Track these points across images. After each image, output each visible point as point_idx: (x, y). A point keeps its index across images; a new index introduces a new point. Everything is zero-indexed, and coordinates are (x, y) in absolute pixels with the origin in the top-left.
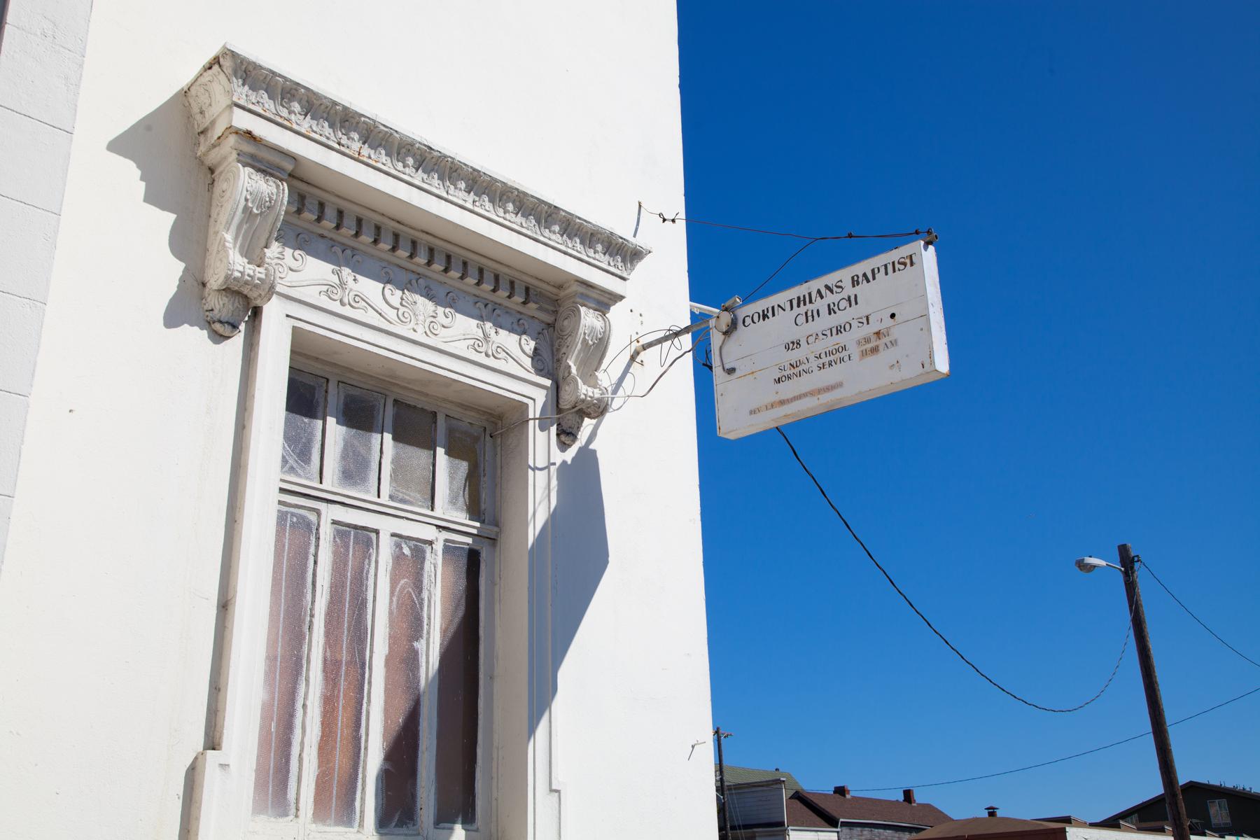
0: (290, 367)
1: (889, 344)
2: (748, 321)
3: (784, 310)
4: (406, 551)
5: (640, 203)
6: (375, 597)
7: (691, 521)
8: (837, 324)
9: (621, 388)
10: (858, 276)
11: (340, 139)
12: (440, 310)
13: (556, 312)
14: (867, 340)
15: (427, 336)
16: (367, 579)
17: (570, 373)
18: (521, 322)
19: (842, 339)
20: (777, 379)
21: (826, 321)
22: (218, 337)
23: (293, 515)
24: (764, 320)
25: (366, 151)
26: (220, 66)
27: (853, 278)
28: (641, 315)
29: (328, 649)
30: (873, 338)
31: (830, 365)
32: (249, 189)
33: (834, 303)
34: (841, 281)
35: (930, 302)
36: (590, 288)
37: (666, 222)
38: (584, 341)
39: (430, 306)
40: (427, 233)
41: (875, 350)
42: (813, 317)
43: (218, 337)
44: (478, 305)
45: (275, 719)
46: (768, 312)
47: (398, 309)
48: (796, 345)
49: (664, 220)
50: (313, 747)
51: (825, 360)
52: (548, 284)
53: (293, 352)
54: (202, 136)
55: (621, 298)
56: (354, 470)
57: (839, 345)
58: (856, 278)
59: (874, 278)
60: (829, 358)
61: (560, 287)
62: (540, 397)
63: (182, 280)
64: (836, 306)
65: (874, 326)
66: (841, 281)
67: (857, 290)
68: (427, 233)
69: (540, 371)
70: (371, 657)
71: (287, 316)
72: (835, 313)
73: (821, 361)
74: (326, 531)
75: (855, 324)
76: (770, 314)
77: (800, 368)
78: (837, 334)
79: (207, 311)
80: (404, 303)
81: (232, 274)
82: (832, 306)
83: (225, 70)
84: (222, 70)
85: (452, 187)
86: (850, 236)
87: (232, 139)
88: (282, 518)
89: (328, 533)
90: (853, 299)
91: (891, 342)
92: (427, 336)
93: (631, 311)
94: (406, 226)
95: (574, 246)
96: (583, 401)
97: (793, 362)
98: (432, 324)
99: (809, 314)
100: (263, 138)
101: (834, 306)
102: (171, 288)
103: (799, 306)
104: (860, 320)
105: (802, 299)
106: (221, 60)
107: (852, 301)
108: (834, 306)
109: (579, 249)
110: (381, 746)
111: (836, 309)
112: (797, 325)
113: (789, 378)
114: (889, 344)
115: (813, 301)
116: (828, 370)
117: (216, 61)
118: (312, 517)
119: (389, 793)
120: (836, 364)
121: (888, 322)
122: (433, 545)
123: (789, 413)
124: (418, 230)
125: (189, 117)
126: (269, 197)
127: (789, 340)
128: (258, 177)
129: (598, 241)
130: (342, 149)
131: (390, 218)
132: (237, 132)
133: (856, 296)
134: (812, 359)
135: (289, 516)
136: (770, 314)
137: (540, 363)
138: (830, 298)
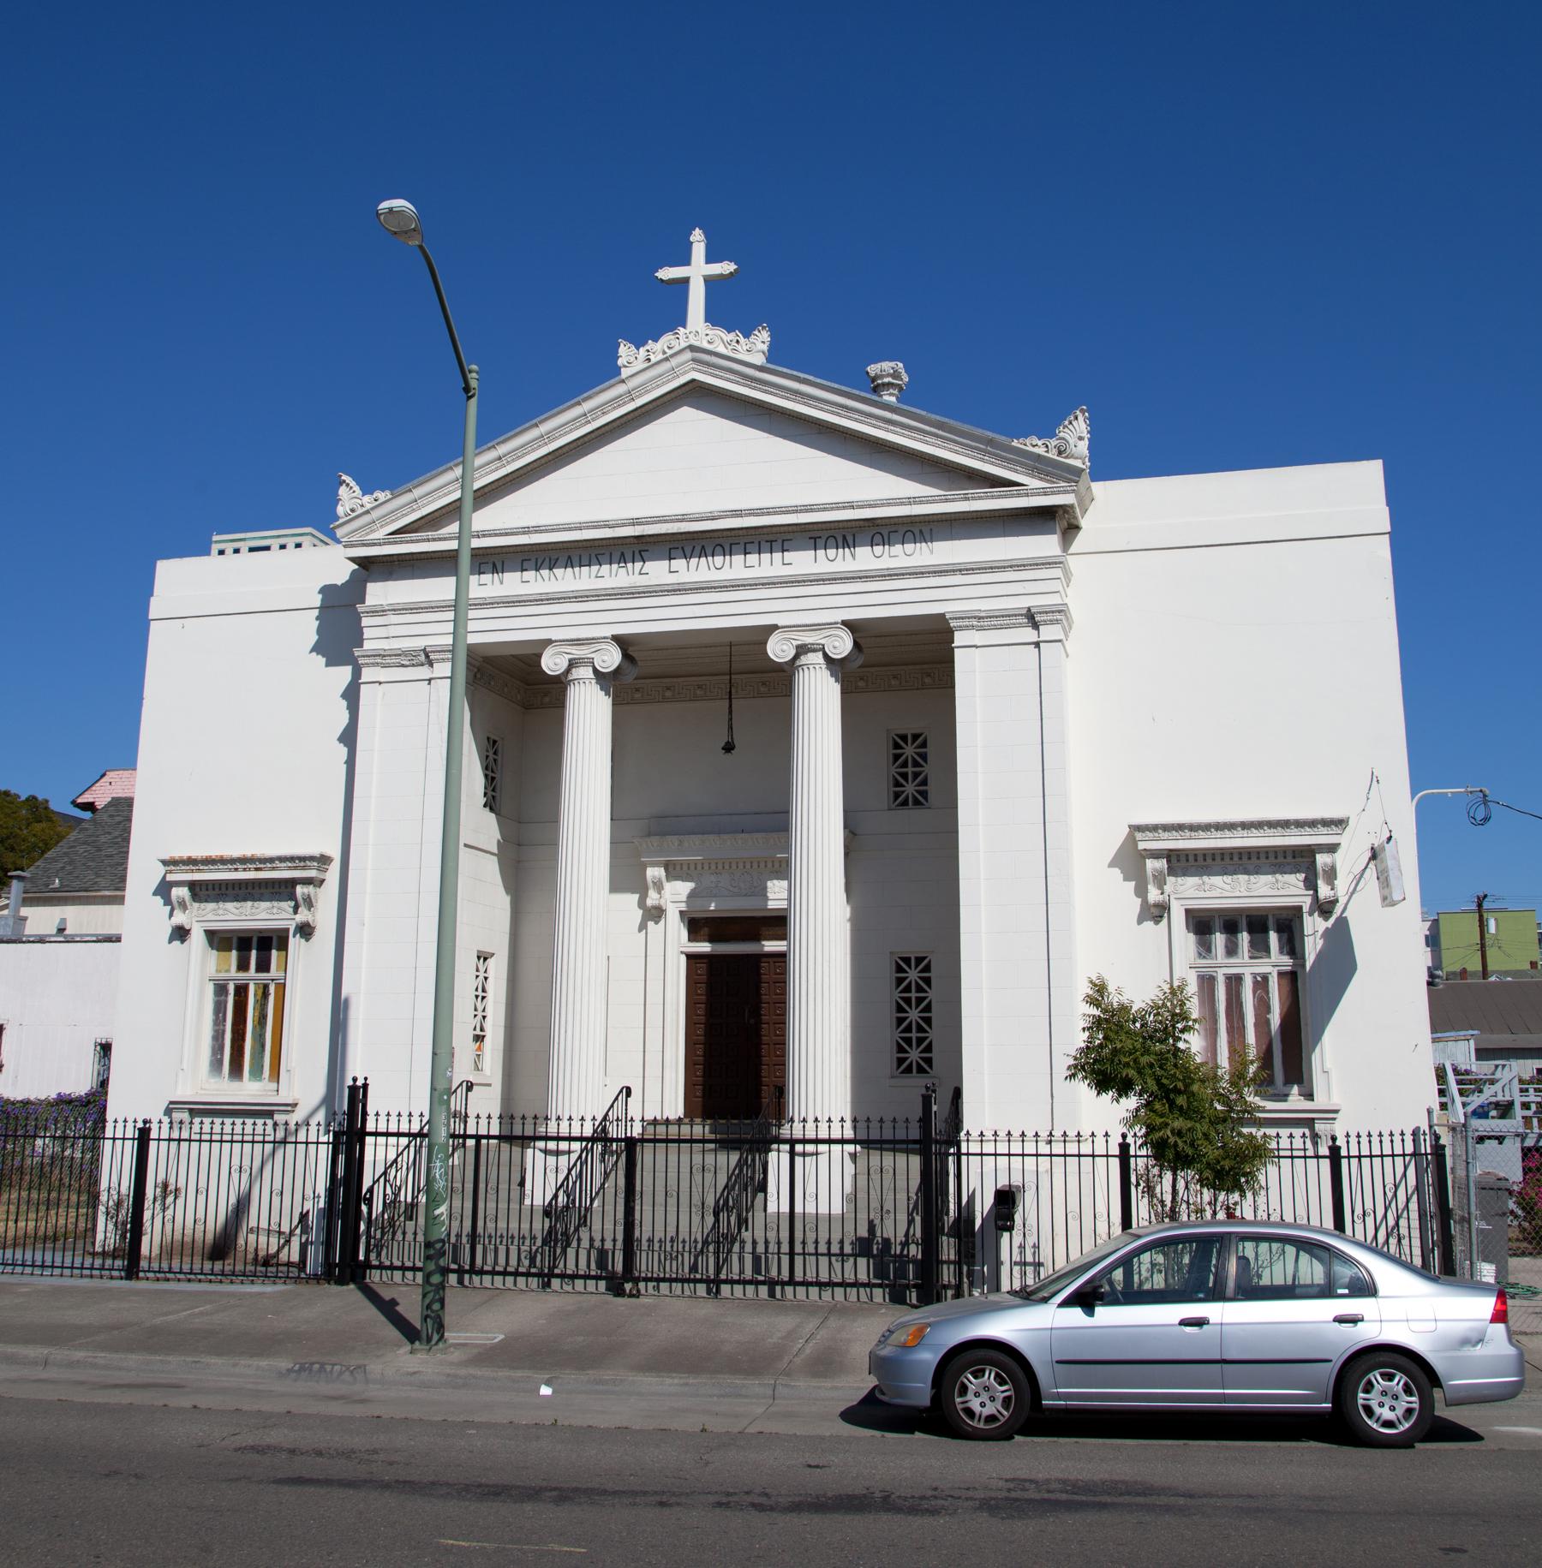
4: (1259, 979)
11: (296, 909)
12: (1252, 877)
22: (1157, 923)
25: (1193, 834)
38: (1323, 870)
39: (1246, 877)
43: (1157, 923)
56: (1231, 950)
62: (1308, 900)
63: (1141, 905)
69: (1307, 888)
91: (1187, 860)
102: (1137, 909)
118: (1215, 974)
128: (1156, 861)
129: (1264, 825)
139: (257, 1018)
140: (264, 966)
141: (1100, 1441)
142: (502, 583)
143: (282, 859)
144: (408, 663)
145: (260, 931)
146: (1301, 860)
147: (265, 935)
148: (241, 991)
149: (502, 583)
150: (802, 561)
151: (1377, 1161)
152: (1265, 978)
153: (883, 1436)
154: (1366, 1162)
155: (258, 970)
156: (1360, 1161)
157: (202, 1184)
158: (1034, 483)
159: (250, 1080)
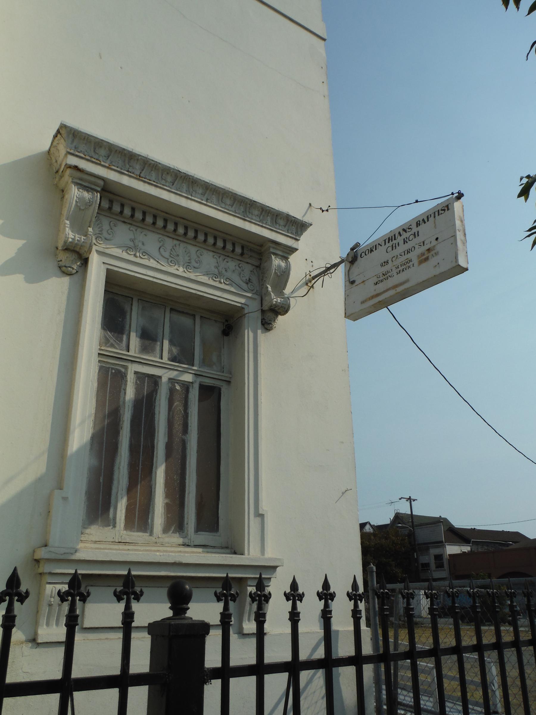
0: (105, 291)
1: (434, 255)
2: (363, 254)
3: (381, 246)
4: (178, 387)
7: (343, 370)
8: (406, 249)
10: (419, 221)
13: (261, 259)
14: (423, 254)
15: (186, 272)
16: (155, 403)
17: (268, 290)
18: (240, 265)
19: (409, 256)
20: (375, 283)
21: (402, 248)
23: (112, 369)
24: (371, 253)
26: (60, 134)
27: (417, 223)
28: (312, 262)
30: (426, 253)
31: (403, 271)
32: (77, 196)
33: (407, 238)
34: (411, 225)
35: (457, 228)
36: (277, 245)
37: (324, 212)
38: (275, 273)
40: (183, 219)
41: (427, 259)
42: (396, 246)
44: (215, 256)
45: (102, 475)
46: (373, 248)
47: (168, 259)
48: (386, 263)
49: (323, 211)
50: (124, 490)
51: (401, 268)
52: (254, 244)
53: (107, 282)
54: (57, 174)
55: (296, 250)
57: (408, 260)
58: (418, 222)
59: (428, 220)
60: (403, 267)
61: (261, 246)
64: (408, 239)
65: (427, 247)
66: (411, 225)
68: (183, 219)
70: (157, 444)
71: (104, 263)
72: (407, 242)
73: (398, 270)
74: (131, 378)
75: (417, 247)
76: (374, 249)
77: (388, 275)
78: (408, 253)
79: (58, 261)
80: (171, 256)
81: (68, 240)
82: (406, 239)
83: (63, 136)
84: (62, 137)
85: (194, 192)
86: (417, 201)
87: (68, 171)
88: (101, 368)
89: (132, 378)
90: (416, 234)
92: (186, 272)
93: (306, 260)
94: (171, 215)
95: (266, 222)
96: (275, 305)
97: (384, 273)
98: (188, 267)
99: (394, 245)
100: (84, 169)
101: (407, 239)
103: (389, 242)
104: (420, 244)
105: (391, 238)
106: (60, 130)
108: (407, 239)
109: (270, 224)
110: (164, 490)
111: (408, 240)
112: (387, 252)
113: (382, 281)
114: (434, 255)
115: (396, 238)
116: (402, 274)
117: (58, 132)
119: (169, 515)
120: (406, 270)
121: (434, 243)
122: (193, 385)
123: (380, 300)
124: (178, 217)
125: (51, 165)
126: (89, 200)
127: (383, 262)
130: (130, 174)
131: (161, 211)
132: (70, 167)
133: (418, 232)
134: (394, 268)
135: (110, 369)
136: (374, 249)
137: (252, 287)
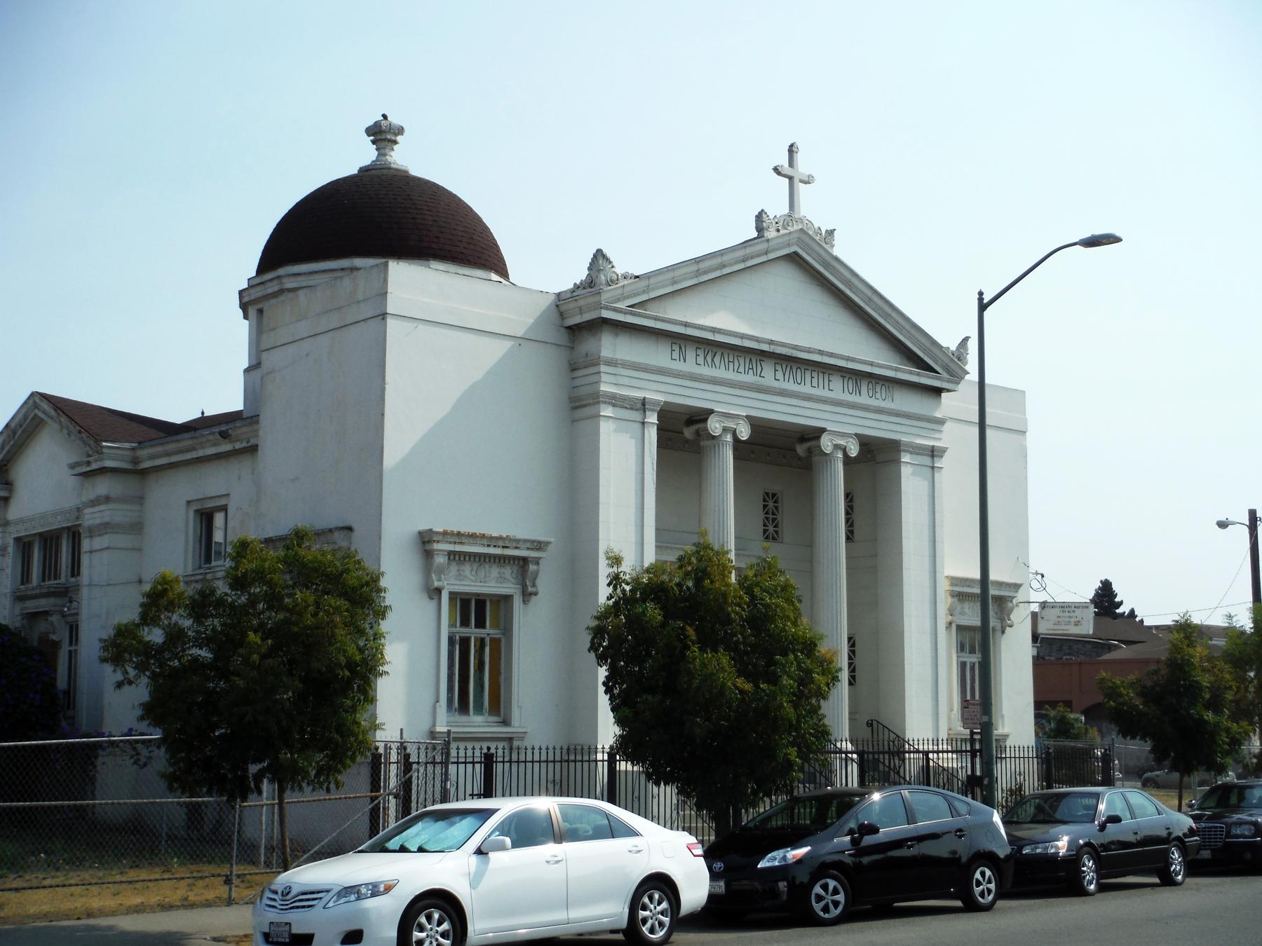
5: (1111, 239)
6: (299, 274)
9: (1248, 524)
29: (360, 849)
41: (1077, 625)
67: (1076, 609)
107: (1074, 612)
138: (1069, 609)
139: (477, 665)
140: (480, 624)
141: (761, 933)
142: (685, 361)
143: (473, 536)
144: (628, 406)
145: (478, 595)
146: (522, 563)
147: (481, 598)
148: (465, 642)
149: (685, 361)
150: (837, 389)
151: (543, 765)
152: (974, 664)
153: (1035, 903)
154: (1017, 760)
155: (477, 627)
156: (474, 765)
157: (1022, 770)
158: (945, 375)
159: (474, 714)
